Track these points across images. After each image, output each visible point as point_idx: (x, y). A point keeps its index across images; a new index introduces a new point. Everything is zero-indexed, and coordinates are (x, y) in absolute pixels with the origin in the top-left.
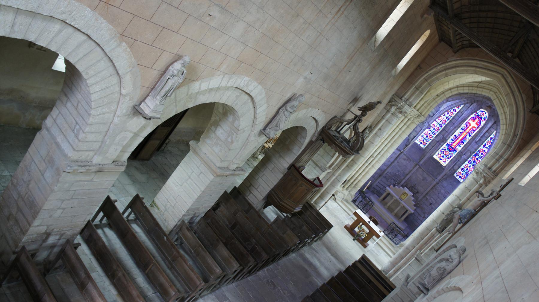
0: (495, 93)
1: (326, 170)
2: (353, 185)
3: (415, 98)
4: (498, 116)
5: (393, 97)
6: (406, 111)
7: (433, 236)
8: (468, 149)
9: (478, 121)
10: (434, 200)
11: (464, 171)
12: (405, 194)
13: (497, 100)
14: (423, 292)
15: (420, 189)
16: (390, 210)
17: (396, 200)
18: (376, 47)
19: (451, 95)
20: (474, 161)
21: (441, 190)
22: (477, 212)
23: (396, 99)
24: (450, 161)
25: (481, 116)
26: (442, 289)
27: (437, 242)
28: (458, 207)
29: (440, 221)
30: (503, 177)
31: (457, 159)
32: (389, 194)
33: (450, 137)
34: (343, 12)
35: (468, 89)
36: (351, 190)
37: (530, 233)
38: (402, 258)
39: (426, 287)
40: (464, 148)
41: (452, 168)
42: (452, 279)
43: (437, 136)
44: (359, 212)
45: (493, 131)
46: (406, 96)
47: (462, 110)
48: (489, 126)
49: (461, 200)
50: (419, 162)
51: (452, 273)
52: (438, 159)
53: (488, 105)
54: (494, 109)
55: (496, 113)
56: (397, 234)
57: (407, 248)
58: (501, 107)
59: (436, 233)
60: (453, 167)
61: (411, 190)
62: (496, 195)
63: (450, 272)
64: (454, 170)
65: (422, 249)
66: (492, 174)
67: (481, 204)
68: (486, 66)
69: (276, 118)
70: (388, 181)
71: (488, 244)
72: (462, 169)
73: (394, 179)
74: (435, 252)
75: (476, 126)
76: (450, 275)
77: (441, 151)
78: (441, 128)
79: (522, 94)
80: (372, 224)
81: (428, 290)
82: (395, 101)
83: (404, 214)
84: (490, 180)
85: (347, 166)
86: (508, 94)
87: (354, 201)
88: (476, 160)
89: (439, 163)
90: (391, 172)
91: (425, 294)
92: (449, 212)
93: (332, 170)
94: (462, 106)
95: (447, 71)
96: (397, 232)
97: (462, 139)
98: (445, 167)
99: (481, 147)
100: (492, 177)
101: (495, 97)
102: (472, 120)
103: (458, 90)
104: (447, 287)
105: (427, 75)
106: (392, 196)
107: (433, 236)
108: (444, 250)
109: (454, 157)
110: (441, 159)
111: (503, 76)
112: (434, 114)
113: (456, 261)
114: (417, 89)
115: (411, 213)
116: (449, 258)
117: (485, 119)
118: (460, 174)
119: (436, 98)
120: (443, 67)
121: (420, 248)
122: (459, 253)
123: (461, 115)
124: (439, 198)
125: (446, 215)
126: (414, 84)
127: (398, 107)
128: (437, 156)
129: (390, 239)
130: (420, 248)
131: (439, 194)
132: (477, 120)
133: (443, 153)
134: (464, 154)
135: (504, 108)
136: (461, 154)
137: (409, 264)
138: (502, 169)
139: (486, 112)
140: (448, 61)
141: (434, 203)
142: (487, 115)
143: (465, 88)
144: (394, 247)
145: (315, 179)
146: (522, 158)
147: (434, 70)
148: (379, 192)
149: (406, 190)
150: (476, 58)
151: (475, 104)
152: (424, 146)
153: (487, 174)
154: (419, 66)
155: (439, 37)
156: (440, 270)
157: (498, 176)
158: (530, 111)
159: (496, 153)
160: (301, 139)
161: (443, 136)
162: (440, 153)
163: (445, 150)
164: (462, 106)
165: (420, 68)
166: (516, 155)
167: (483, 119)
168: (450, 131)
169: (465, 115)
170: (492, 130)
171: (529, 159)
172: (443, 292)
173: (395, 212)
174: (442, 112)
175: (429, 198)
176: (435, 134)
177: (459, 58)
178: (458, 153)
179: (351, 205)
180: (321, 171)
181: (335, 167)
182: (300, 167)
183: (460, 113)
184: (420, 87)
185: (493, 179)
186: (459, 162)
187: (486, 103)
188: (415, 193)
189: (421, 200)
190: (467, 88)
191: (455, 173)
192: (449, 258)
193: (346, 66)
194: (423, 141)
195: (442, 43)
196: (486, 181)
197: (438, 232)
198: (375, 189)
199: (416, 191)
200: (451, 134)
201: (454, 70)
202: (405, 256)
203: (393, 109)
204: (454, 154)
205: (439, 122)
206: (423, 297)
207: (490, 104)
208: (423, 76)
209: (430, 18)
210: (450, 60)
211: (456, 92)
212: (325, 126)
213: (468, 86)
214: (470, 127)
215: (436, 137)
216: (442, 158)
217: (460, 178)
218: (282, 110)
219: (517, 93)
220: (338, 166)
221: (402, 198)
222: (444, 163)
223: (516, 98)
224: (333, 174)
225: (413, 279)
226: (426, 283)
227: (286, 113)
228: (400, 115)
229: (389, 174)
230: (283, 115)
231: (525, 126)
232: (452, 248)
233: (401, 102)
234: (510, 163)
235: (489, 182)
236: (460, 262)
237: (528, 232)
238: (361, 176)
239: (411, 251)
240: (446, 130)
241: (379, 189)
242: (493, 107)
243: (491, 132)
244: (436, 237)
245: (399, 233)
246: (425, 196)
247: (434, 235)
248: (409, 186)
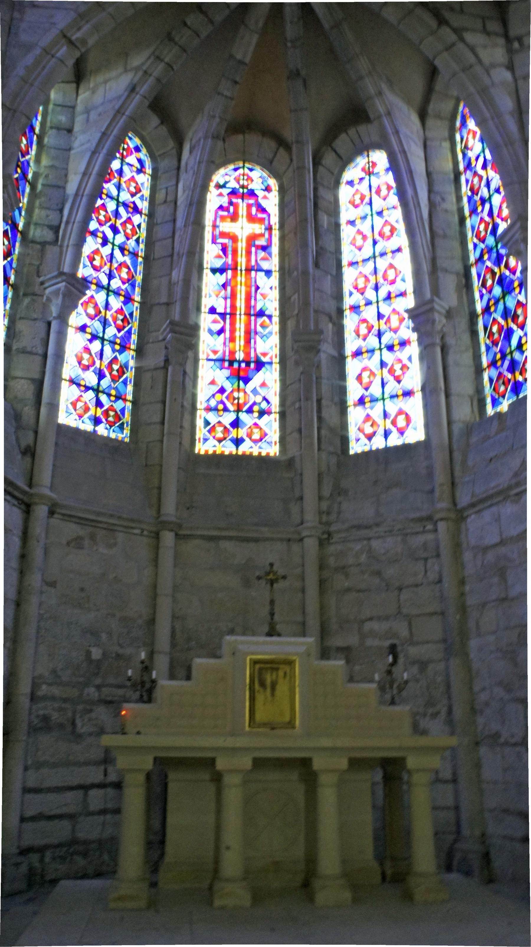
9: (249, 206)
10: (387, 618)
21: (370, 550)
25: (243, 187)
70: (78, 737)
72: (361, 401)
75: (258, 228)
77: (209, 409)
78: (135, 307)
89: (247, 458)
90: (54, 672)
102: (223, 218)
110: (238, 442)
112: (56, 229)
123: (169, 210)
124: (400, 589)
128: (212, 442)
131: (378, 573)
132: (242, 206)
133: (226, 409)
141: (404, 633)
152: (121, 427)
162: (212, 418)
163: (222, 391)
167: (260, 193)
168: (178, 290)
175: (352, 640)
194: (99, 404)
198: (41, 850)
214: (242, 246)
229: (56, 691)
240: (164, 300)
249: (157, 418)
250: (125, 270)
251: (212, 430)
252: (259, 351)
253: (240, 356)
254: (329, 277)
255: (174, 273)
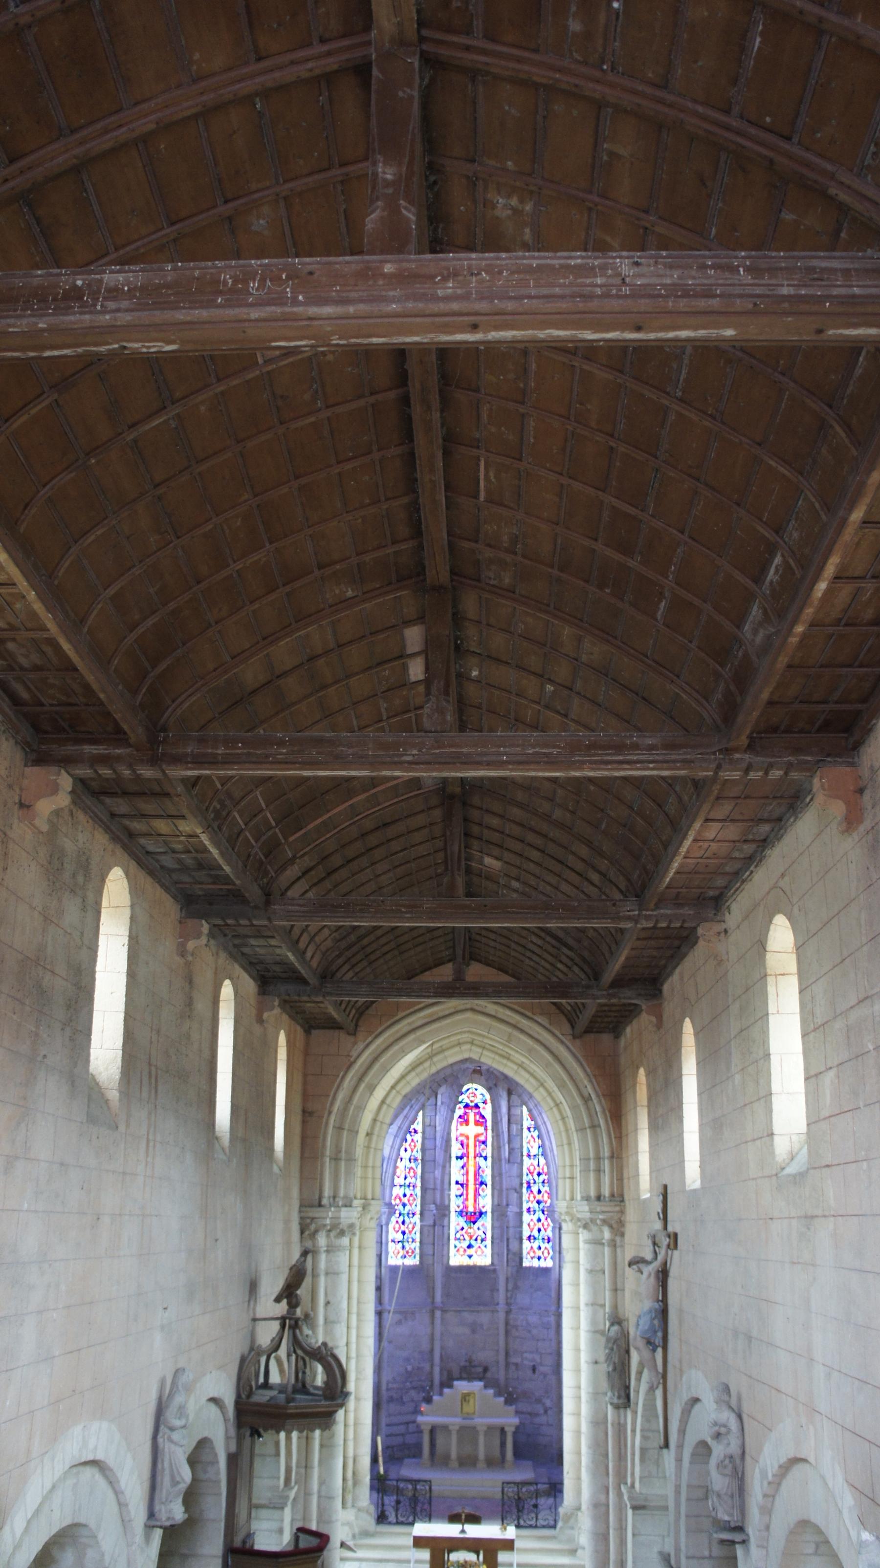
0: (472, 1043)
1: (287, 1497)
2: (350, 1483)
3: (346, 1181)
4: (506, 1077)
5: (303, 1214)
6: (350, 1221)
7: (620, 1429)
8: (504, 1187)
9: (475, 1114)
11: (535, 1238)
12: (465, 1398)
13: (485, 1052)
14: (733, 1543)
15: (483, 1356)
16: (467, 1462)
17: (462, 1429)
18: (227, 1151)
19: (392, 1112)
20: (538, 1202)
22: (664, 1300)
23: (311, 1215)
24: (492, 1242)
25: (472, 1102)
26: (765, 1496)
27: (642, 1430)
28: (612, 1324)
29: (604, 1385)
30: (638, 1195)
31: (501, 1227)
32: (433, 1431)
33: (449, 1195)
34: (155, 1141)
35: (417, 1075)
36: (354, 1500)
37: (799, 1263)
38: (605, 1537)
39: (733, 1525)
40: (496, 1192)
41: (508, 1255)
42: (761, 1461)
43: (422, 1214)
44: (422, 1529)
45: (519, 1113)
46: (327, 1192)
47: (428, 1121)
48: (504, 1109)
49: (604, 1306)
50: (433, 1302)
51: (747, 1450)
52: (464, 1261)
53: (471, 1070)
54: (488, 1070)
55: (498, 1074)
56: (533, 1502)
57: (596, 1505)
58: (505, 1061)
59: (619, 1417)
60: (508, 1250)
61: (470, 1378)
62: (668, 1240)
63: (743, 1453)
64: (514, 1254)
65: (625, 1477)
66: (612, 1203)
67: (657, 1278)
68: (431, 1015)
69: (159, 1466)
70: (404, 1403)
71: (753, 1340)
72: (529, 1238)
73: (414, 1388)
74: (665, 1451)
75: (481, 1129)
76: (748, 1458)
77: (456, 1239)
79: (536, 1018)
80: (474, 1531)
81: (740, 1529)
82: (313, 1219)
83: (503, 1444)
84: (620, 1219)
85: (322, 1446)
86: (510, 1035)
87: (381, 1518)
88: (539, 1197)
90: (394, 1379)
91: (743, 1542)
92: (605, 1348)
93: (296, 1488)
94: (421, 1114)
95: (367, 1079)
96: (531, 1498)
97: (475, 1179)
98: (493, 1264)
99: (525, 1163)
100: (617, 1209)
101: (480, 1050)
103: (398, 1092)
104: (769, 1483)
105: (333, 1118)
106: (445, 1428)
107: (620, 1429)
108: (679, 1431)
109: (493, 1228)
111: (472, 1010)
113: (733, 1424)
114: (336, 1159)
115: (517, 1428)
116: (717, 1428)
117: (485, 1102)
118: (534, 1252)
119: (370, 1141)
120: (352, 1077)
121: (621, 1477)
122: (724, 1401)
124: (538, 1340)
125: (606, 1361)
126: (323, 1155)
127: (329, 1227)
128: (458, 1256)
129: (531, 1526)
130: (621, 1477)
132: (472, 1117)
134: (508, 1205)
135: (511, 1058)
136: (499, 1211)
137: (634, 1535)
138: (621, 1179)
139: (475, 1086)
140: (352, 1059)
142: (481, 1090)
143: (408, 1078)
144: (554, 1538)
145: (297, 1539)
146: (639, 1132)
147: (341, 1096)
148: (404, 1446)
149: (462, 1386)
150: (401, 1015)
151: (442, 1090)
153: (603, 1212)
154: (304, 1111)
155: (302, 1026)
156: (725, 1467)
157: (626, 1198)
158: (574, 1037)
159: (584, 1159)
160: (205, 1472)
161: (434, 1203)
162: (457, 1243)
163: (462, 1229)
164: (421, 1114)
165: (311, 1114)
166: (621, 1133)
167: (481, 1105)
169: (440, 1125)
170: (515, 1111)
171: (654, 1127)
172: (771, 1499)
173: (481, 1455)
174: (394, 1157)
176: (414, 1214)
177: (370, 1039)
178: (493, 1212)
179: (382, 1534)
180: (276, 1514)
181: (297, 1473)
182: (244, 1542)
183: (428, 1129)
184: (340, 1152)
185: (622, 1212)
186: (511, 1231)
187: (464, 1070)
188: (481, 1375)
189: (507, 1379)
190: (413, 1074)
191: (521, 1259)
192: (717, 1428)
193: (206, 1236)
195: (315, 1032)
196: (615, 1226)
197: (622, 1411)
199: (480, 1370)
200: (446, 1186)
201: (377, 1066)
202: (608, 1527)
203: (322, 1240)
204: (487, 1222)
205: (402, 1183)
206: (747, 1551)
207: (472, 1067)
208: (327, 1124)
209: (274, 1014)
210: (354, 1054)
211: (399, 1099)
212: (238, 1396)
213: (413, 1069)
214: (471, 1142)
215: (422, 1220)
216: (470, 1251)
217: (542, 1260)
218: (163, 1436)
219: (524, 1023)
220: (304, 1464)
221: (468, 1414)
222: (483, 1258)
223: (531, 1032)
224: (307, 1494)
225: (680, 1550)
226: (726, 1518)
227: (175, 1436)
228: (345, 1241)
229: (395, 1386)
230: (172, 1446)
231: (588, 1070)
232: (690, 1412)
233: (328, 1212)
234: (624, 1155)
235: (621, 1223)
236: (740, 1417)
237: (794, 1263)
238: (351, 1444)
239: (608, 1506)
241: (399, 1440)
242: (484, 1068)
243: (519, 1118)
244: (626, 1423)
245: (537, 1494)
246: (507, 1365)
247: (619, 1424)
248: (456, 1372)
249: (431, 1252)
250: (412, 1171)
251: (458, 1250)
252: (481, 1205)
253: (471, 1209)
254: (764, 519)
255: (436, 1172)
